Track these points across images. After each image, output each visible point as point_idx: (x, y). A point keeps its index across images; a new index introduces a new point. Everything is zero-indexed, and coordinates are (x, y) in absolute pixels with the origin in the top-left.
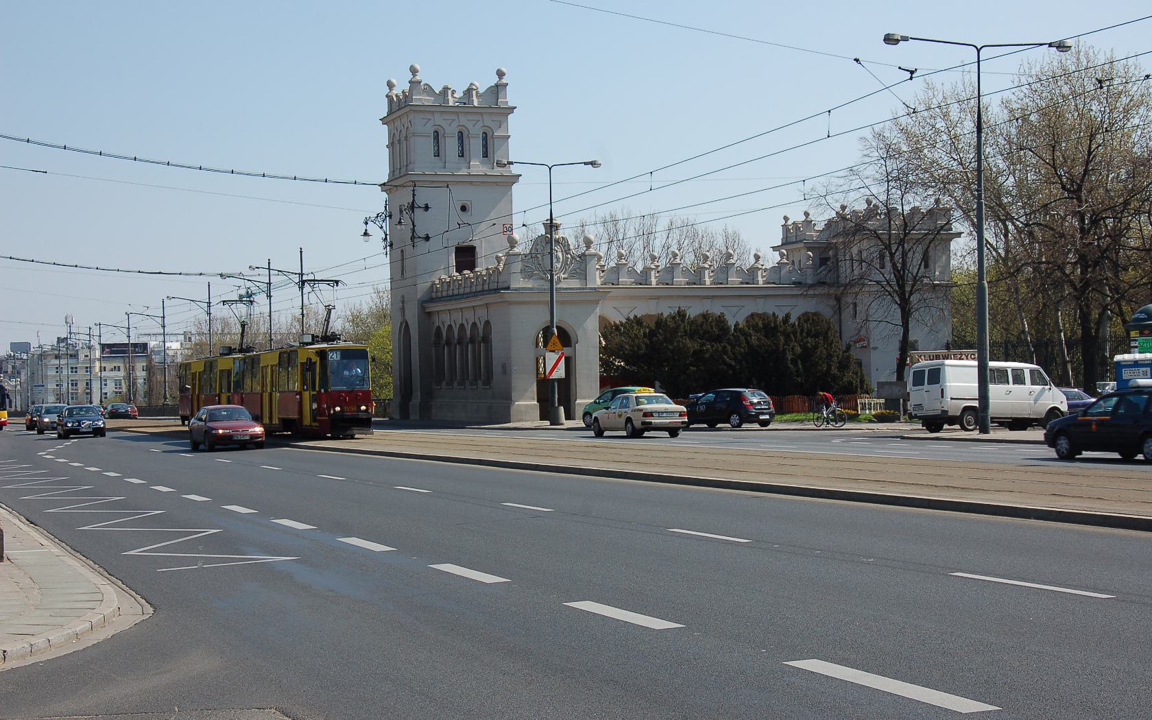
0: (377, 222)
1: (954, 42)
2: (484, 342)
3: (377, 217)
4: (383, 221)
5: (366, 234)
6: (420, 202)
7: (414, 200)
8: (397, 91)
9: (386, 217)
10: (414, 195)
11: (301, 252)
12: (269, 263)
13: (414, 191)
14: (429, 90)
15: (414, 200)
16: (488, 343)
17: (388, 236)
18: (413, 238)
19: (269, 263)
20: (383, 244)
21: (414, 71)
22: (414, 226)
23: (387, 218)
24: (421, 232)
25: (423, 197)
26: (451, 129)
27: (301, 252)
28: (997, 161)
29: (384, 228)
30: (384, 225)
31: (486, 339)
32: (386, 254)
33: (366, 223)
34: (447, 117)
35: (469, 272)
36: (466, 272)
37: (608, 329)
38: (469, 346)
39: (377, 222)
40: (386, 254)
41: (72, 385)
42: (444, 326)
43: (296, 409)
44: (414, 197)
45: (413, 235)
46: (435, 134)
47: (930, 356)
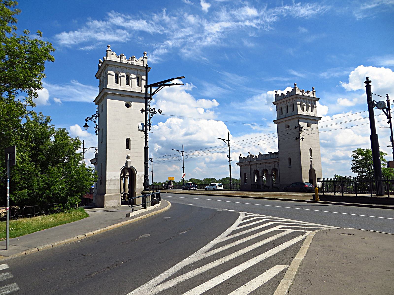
3: (92, 117)
5: (86, 126)
29: (96, 122)
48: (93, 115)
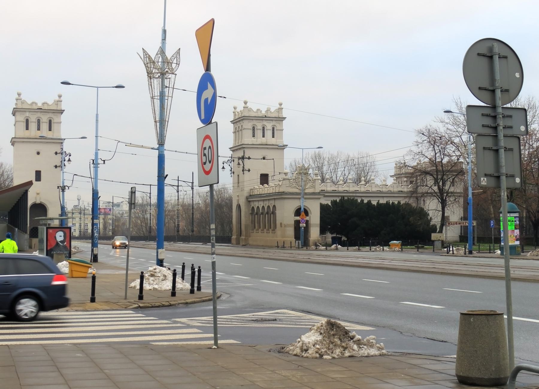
0: (228, 163)
1: (203, 128)
2: (257, 214)
3: (228, 161)
4: (231, 163)
6: (247, 156)
7: (244, 155)
8: (238, 110)
9: (231, 161)
10: (244, 153)
11: (193, 174)
12: (178, 178)
13: (244, 151)
14: (250, 110)
15: (244, 155)
16: (274, 214)
17: (232, 169)
18: (243, 171)
19: (178, 178)
20: (230, 172)
21: (246, 103)
22: (244, 165)
23: (232, 162)
24: (246, 168)
25: (248, 153)
26: (259, 126)
27: (193, 174)
28: (310, 158)
29: (231, 166)
30: (231, 164)
31: (274, 213)
32: (231, 176)
33: (223, 164)
34: (278, 122)
35: (267, 185)
36: (265, 185)
37: (324, 208)
38: (256, 215)
39: (228, 163)
40: (231, 176)
41: (86, 230)
42: (266, 206)
43: (277, 243)
44: (244, 154)
45: (243, 169)
46: (263, 128)
47: (453, 223)
48: (228, 160)
